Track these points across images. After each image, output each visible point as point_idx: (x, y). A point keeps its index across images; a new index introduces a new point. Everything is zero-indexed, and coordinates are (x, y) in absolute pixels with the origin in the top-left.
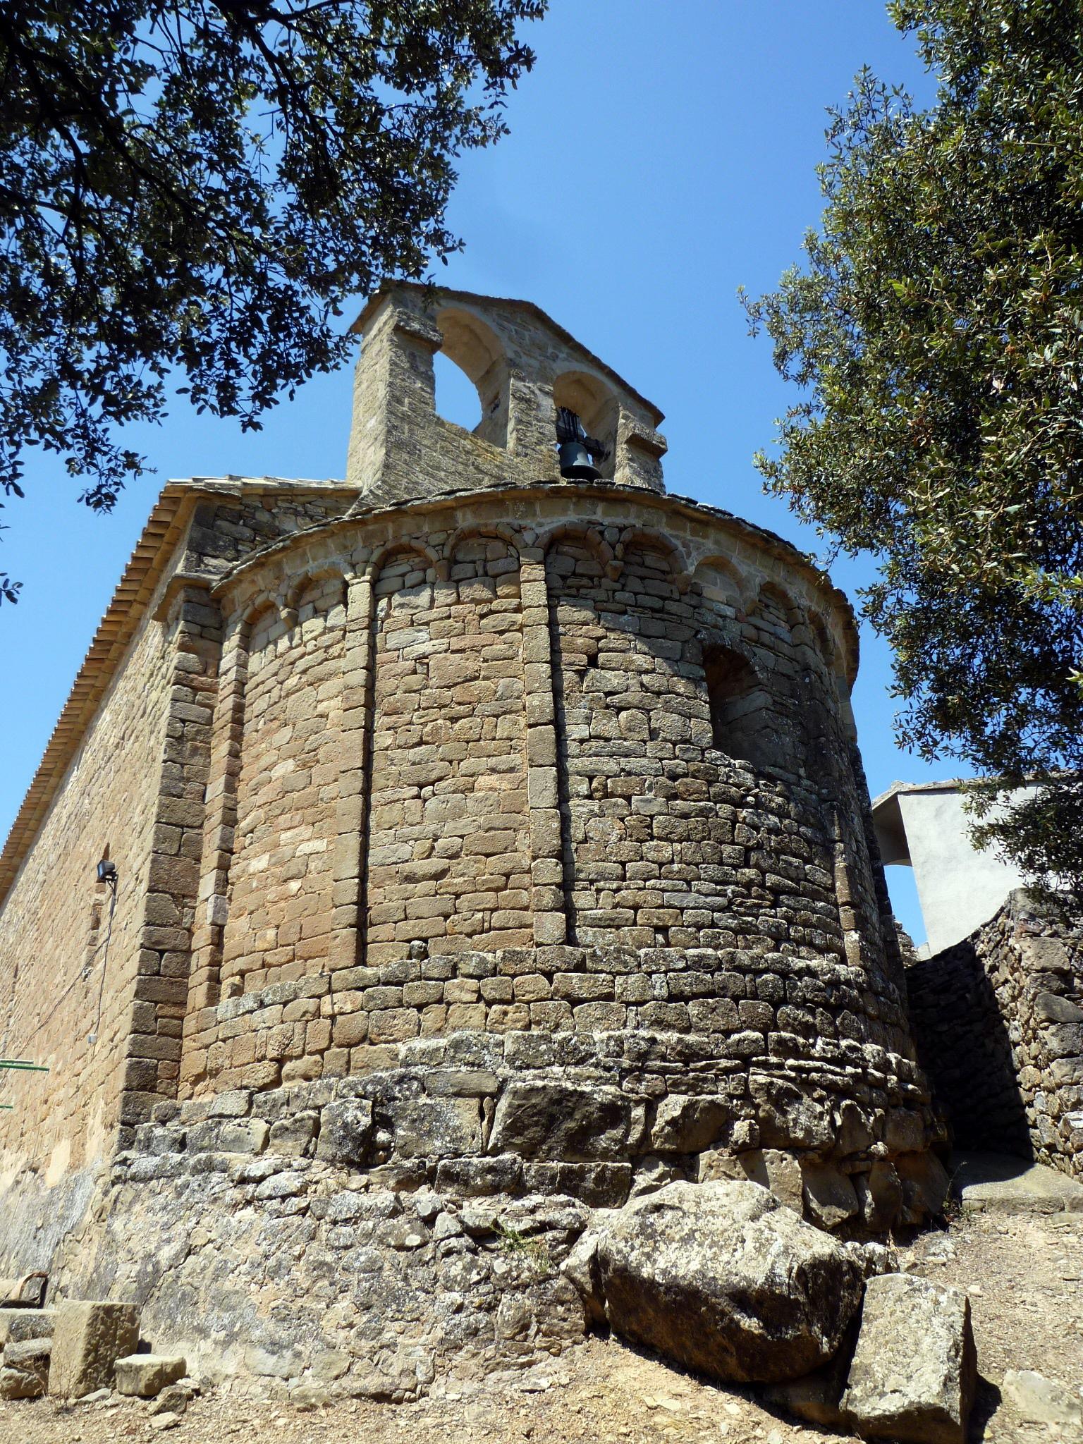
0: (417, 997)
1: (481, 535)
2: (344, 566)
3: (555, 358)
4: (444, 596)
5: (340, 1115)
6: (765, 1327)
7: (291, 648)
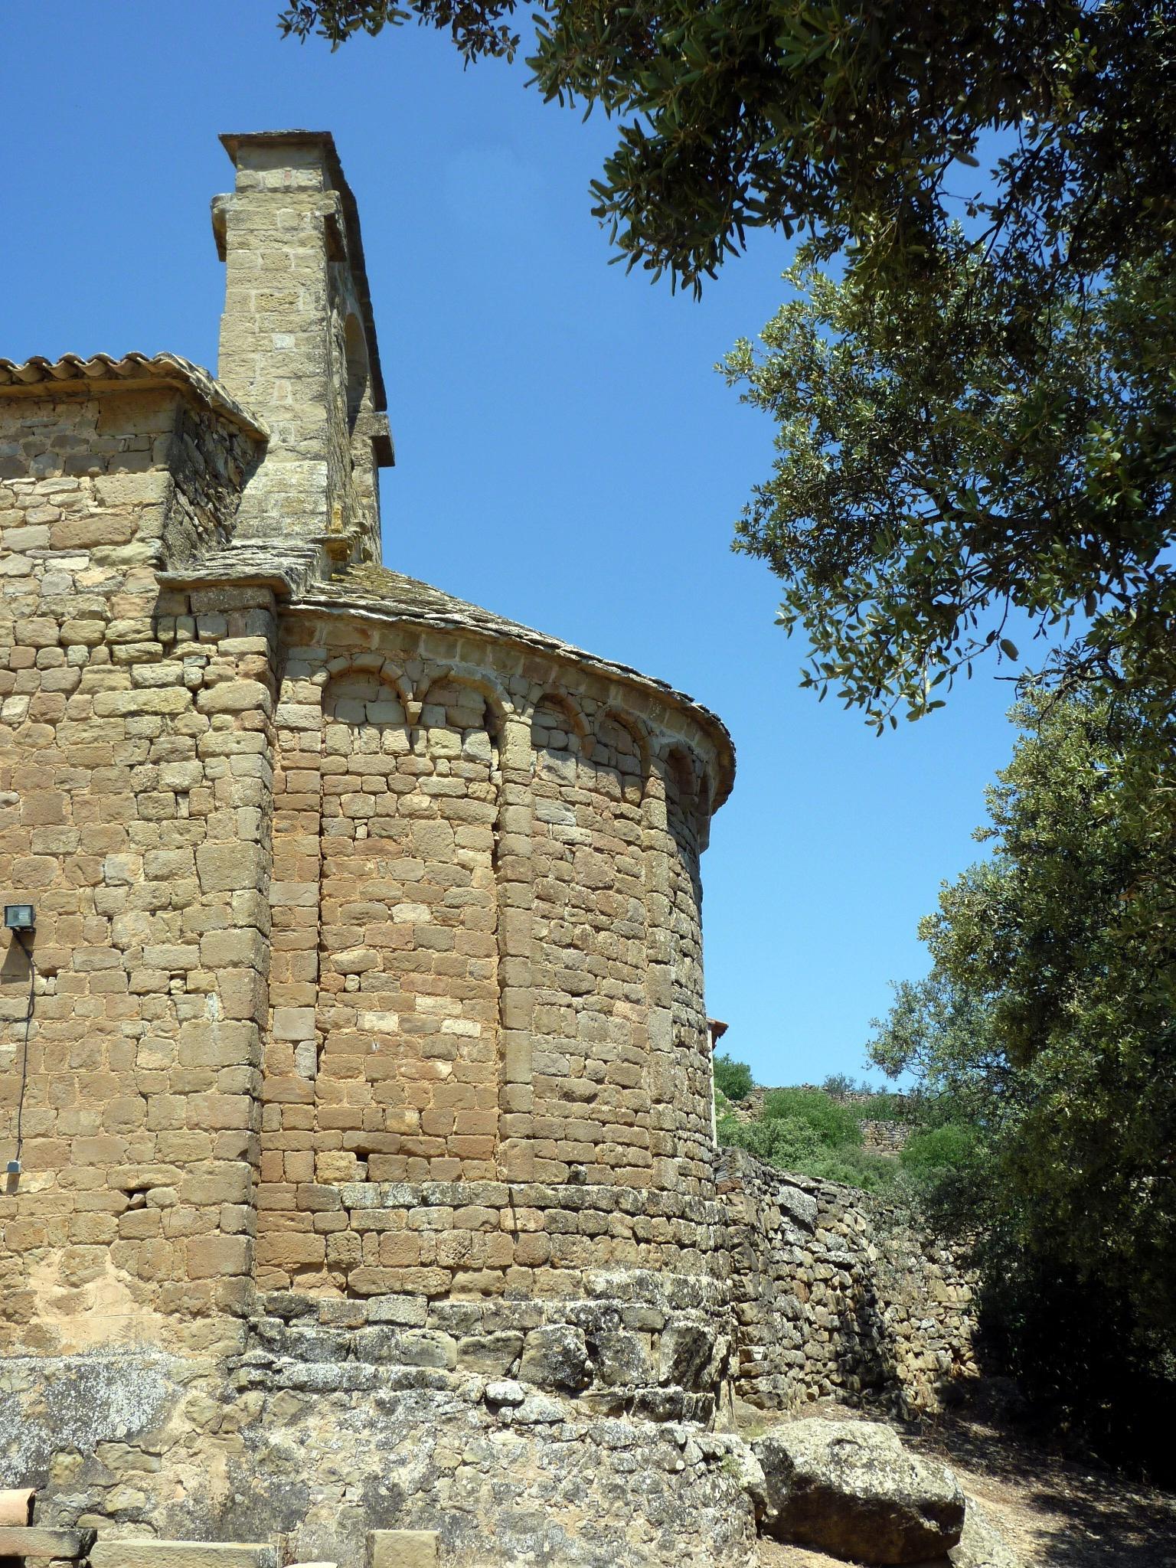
0: (591, 1227)
5: (559, 1341)
6: (940, 1528)
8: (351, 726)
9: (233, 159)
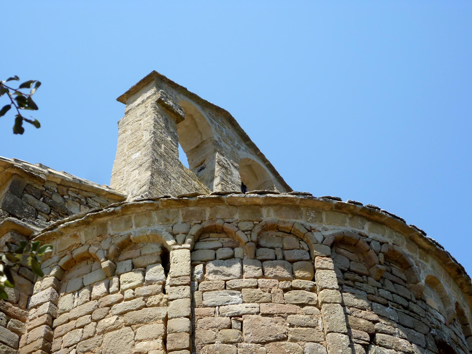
1: (278, 229)
2: (165, 234)
3: (239, 149)
4: (252, 270)
7: (108, 293)
8: (74, 293)
9: (125, 103)
